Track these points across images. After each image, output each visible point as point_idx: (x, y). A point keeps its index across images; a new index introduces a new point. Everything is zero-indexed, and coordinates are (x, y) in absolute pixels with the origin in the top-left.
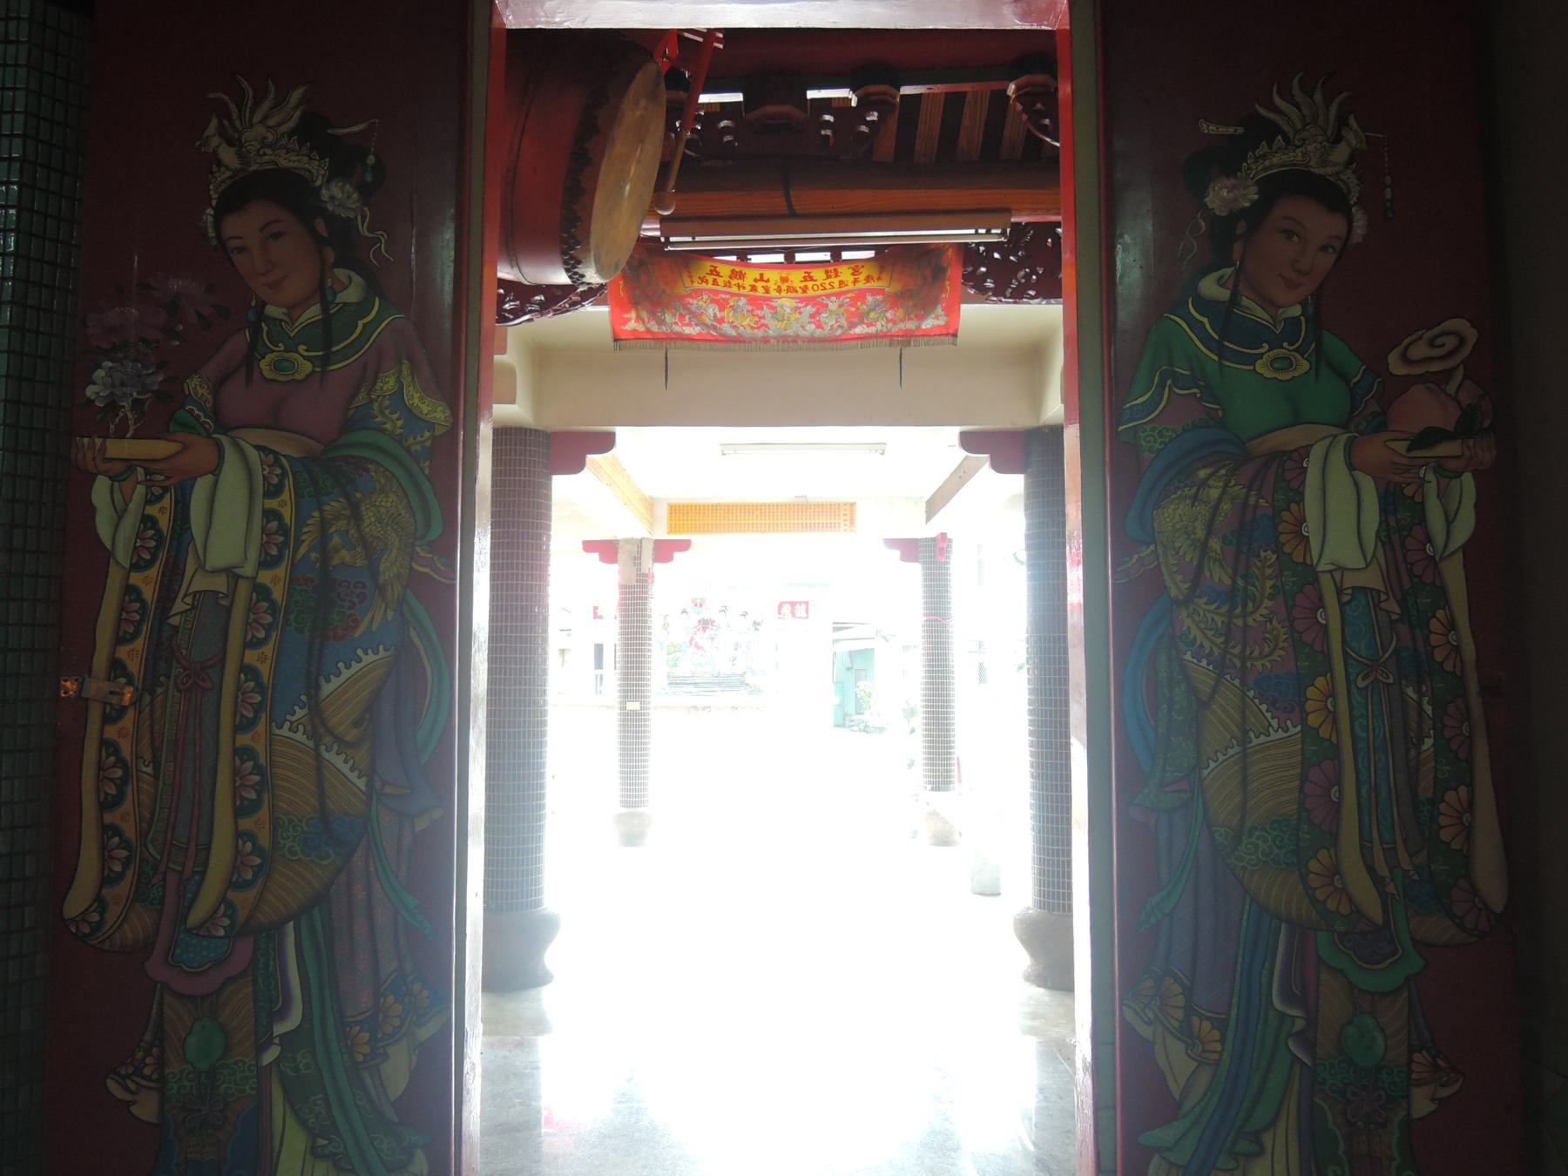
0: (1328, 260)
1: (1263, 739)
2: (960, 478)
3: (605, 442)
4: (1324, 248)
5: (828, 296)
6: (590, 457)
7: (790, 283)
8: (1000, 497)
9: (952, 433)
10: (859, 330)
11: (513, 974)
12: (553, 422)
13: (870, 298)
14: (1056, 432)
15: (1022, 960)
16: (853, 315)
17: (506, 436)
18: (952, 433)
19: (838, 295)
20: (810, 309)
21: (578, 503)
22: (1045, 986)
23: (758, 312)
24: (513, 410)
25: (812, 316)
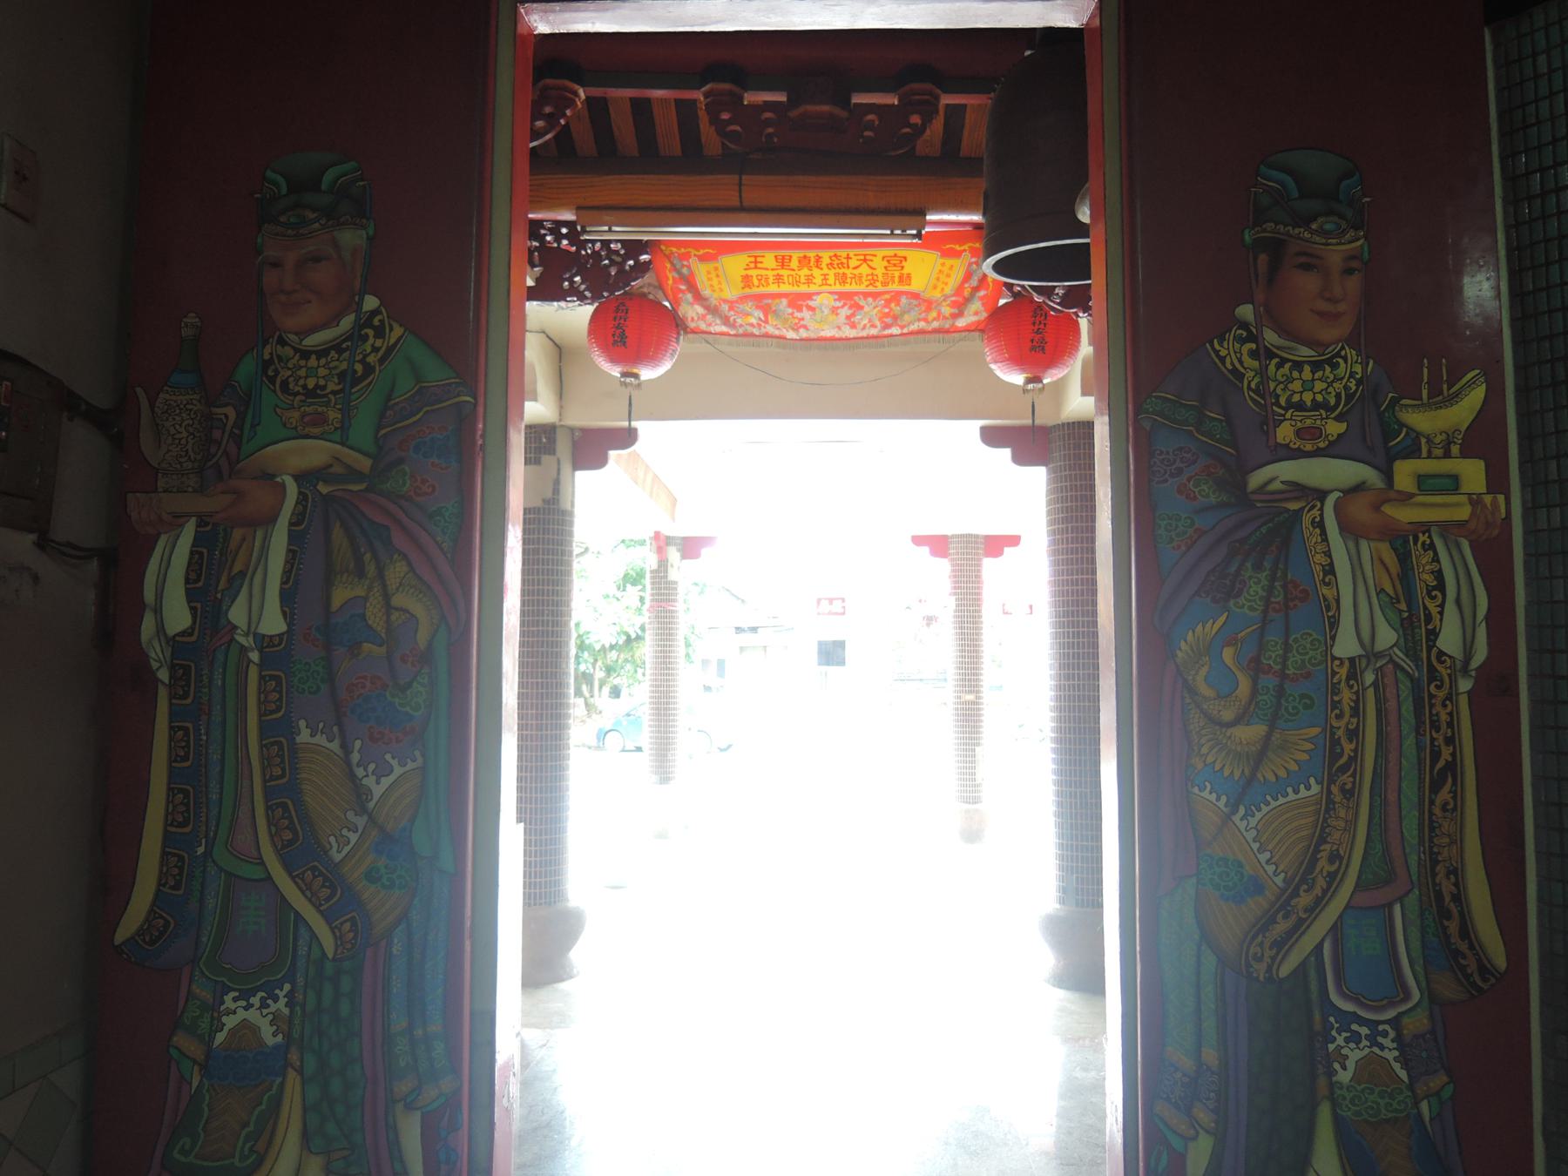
0: (1354, 284)
1: (1282, 800)
2: (642, 543)
3: (626, 438)
4: (1349, 271)
5: (866, 295)
6: (612, 454)
7: (733, 267)
8: (1022, 496)
9: (973, 427)
10: (895, 330)
11: (544, 967)
12: (580, 418)
13: (904, 300)
14: (1086, 427)
15: (1046, 959)
16: (887, 315)
17: (542, 439)
18: (973, 427)
19: (875, 295)
20: (845, 312)
21: (601, 502)
22: (1068, 988)
23: (797, 314)
24: (538, 409)
25: (848, 318)
